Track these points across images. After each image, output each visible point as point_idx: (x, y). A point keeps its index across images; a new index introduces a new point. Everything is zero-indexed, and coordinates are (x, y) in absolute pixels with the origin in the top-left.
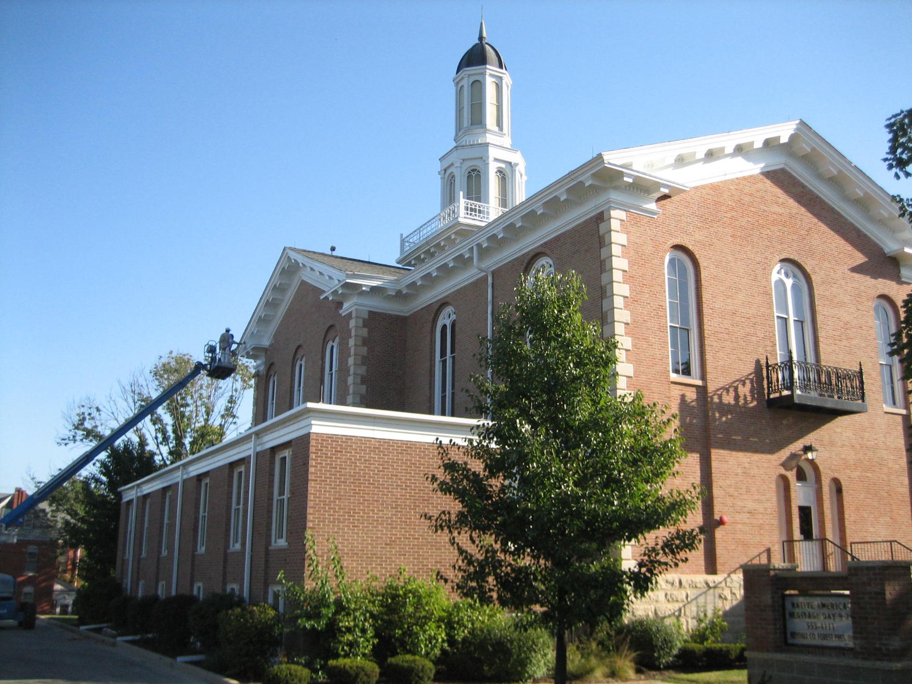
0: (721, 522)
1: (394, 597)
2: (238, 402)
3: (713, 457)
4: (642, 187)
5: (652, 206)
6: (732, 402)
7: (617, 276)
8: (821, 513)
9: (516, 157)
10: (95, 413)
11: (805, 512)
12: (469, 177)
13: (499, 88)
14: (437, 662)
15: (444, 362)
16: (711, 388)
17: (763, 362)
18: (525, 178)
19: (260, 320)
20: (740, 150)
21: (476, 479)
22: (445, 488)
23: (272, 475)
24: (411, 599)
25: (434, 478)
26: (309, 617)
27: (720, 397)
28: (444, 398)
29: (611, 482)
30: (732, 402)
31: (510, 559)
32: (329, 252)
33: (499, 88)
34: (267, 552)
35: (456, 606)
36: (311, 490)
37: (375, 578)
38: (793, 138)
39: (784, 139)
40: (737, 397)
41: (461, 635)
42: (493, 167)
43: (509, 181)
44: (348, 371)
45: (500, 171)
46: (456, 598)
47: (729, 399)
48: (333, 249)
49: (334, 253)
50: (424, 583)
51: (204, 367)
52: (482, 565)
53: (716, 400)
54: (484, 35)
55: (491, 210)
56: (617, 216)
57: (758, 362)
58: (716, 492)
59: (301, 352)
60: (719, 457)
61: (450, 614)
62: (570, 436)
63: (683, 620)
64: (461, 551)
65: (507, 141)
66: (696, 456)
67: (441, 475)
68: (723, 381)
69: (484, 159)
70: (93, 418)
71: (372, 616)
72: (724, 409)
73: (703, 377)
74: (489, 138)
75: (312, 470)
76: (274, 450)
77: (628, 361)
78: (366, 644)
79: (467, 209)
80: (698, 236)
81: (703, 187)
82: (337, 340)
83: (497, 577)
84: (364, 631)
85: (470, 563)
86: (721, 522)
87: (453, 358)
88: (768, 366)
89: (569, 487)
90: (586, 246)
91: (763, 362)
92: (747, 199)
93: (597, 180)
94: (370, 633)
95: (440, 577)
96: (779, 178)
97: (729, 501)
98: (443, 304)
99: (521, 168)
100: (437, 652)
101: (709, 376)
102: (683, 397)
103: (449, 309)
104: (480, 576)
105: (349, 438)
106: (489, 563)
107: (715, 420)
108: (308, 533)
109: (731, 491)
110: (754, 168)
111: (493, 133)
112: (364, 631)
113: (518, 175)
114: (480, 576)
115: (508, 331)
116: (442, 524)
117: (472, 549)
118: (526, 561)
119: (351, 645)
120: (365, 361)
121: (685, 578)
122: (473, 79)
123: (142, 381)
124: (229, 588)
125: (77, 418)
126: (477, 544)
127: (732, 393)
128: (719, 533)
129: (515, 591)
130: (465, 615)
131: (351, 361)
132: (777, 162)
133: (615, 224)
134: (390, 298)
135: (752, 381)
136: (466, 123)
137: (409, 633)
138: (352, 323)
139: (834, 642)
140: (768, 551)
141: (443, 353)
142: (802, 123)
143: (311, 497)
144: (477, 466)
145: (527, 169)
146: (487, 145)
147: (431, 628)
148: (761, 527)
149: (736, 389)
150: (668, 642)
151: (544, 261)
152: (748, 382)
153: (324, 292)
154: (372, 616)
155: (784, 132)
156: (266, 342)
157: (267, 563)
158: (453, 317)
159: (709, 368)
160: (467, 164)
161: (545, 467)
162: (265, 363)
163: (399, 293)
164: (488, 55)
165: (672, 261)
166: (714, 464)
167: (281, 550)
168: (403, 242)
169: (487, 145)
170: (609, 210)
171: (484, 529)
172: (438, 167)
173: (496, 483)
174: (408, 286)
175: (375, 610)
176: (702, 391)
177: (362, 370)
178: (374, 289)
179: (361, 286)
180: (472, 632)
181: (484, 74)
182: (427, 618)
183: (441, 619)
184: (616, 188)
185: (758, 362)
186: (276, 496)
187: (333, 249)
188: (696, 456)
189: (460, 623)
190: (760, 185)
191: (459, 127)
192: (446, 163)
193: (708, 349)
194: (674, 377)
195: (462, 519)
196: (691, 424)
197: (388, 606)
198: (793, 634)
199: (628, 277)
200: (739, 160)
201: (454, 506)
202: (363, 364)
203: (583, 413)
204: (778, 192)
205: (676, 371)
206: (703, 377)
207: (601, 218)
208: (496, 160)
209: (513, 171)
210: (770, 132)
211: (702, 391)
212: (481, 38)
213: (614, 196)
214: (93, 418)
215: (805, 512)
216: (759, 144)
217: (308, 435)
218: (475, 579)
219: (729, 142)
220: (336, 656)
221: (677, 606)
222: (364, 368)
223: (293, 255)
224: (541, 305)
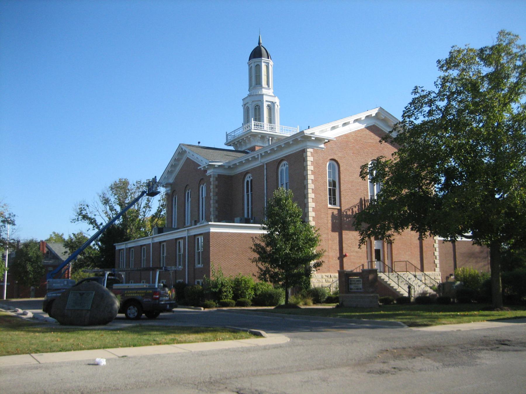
0: (346, 256)
1: (238, 282)
2: (151, 201)
3: (343, 233)
4: (319, 140)
5: (322, 146)
6: (351, 214)
7: (309, 172)
8: (384, 251)
9: (276, 100)
10: (86, 208)
11: (378, 252)
12: (255, 109)
13: (268, 67)
14: (252, 301)
15: (248, 195)
16: (343, 209)
17: (363, 199)
18: (279, 107)
19: (169, 171)
20: (356, 121)
21: (263, 248)
22: (254, 251)
23: (195, 244)
24: (243, 282)
25: (251, 248)
26: (214, 288)
27: (346, 212)
28: (248, 209)
29: (300, 249)
30: (351, 214)
31: (273, 270)
32: (197, 144)
33: (268, 67)
34: (194, 269)
35: (257, 284)
36: (211, 250)
37: (231, 276)
38: (376, 114)
39: (374, 115)
40: (353, 212)
41: (259, 293)
42: (265, 104)
43: (272, 111)
44: (211, 198)
45: (268, 106)
46: (258, 281)
47: (349, 213)
48: (199, 143)
49: (200, 145)
50: (247, 277)
51: (146, 192)
52: (265, 271)
53: (345, 213)
54: (261, 42)
55: (265, 125)
56: (310, 151)
57: (361, 199)
58: (344, 245)
59: (188, 187)
60: (345, 233)
61: (255, 287)
62: (287, 237)
63: (331, 288)
64: (259, 268)
65: (271, 92)
66: (337, 233)
67: (253, 247)
68: (348, 207)
69: (262, 101)
70: (85, 210)
71: (232, 287)
72: (347, 216)
73: (340, 206)
74: (264, 91)
75: (211, 243)
76: (195, 236)
77: (313, 202)
78: (231, 296)
79: (255, 125)
80: (340, 155)
81: (342, 136)
82: (205, 184)
83: (269, 275)
84: (230, 292)
85: (262, 271)
86: (346, 256)
87: (252, 194)
88: (364, 200)
89: (287, 251)
90: (298, 160)
91: (363, 199)
92: (359, 138)
93: (302, 138)
94: (232, 292)
95: (253, 275)
96: (372, 129)
97: (349, 248)
98: (247, 173)
99: (278, 103)
100: (251, 298)
101: (342, 205)
102: (333, 213)
103: (249, 175)
104: (264, 274)
105: (222, 233)
106: (267, 271)
107: (344, 220)
108: (211, 263)
109: (350, 245)
110: (362, 126)
111: (265, 88)
112: (230, 292)
113: (276, 106)
114: (264, 274)
115: (270, 207)
116: (254, 261)
117: (262, 267)
118: (277, 270)
119: (226, 296)
120: (217, 194)
121: (332, 275)
122: (256, 64)
123: (106, 192)
124: (177, 281)
125: (79, 211)
126: (263, 266)
127: (351, 211)
128: (345, 259)
129: (274, 278)
130: (260, 287)
131: (212, 194)
132: (371, 123)
133: (309, 154)
134: (225, 169)
135: (358, 206)
136: (254, 83)
137: (243, 292)
138: (212, 179)
139: (359, 290)
140: (363, 265)
141: (248, 192)
142: (381, 108)
143: (211, 252)
144: (263, 244)
145: (280, 103)
146: (263, 95)
147: (249, 291)
148: (360, 257)
149: (352, 209)
150: (323, 295)
151: (285, 162)
152: (357, 206)
153: (200, 166)
154: (232, 287)
155: (373, 112)
156: (171, 181)
157: (195, 273)
158: (251, 178)
159: (342, 203)
160: (254, 104)
161: (281, 246)
162: (171, 189)
163: (229, 167)
164: (263, 52)
165: (330, 164)
166: (344, 236)
167: (200, 268)
168: (227, 135)
169: (263, 95)
170: (307, 148)
171: (266, 262)
172: (242, 103)
173: (268, 249)
174: (233, 165)
175: (233, 285)
176: (340, 210)
177: (216, 198)
178: (219, 166)
179: (215, 165)
180: (262, 292)
181: (261, 62)
182: (248, 288)
183: (252, 288)
184: (309, 141)
185: (361, 199)
186: (196, 251)
187: (199, 143)
188: (337, 233)
189: (258, 289)
190: (364, 133)
191: (250, 85)
192: (246, 102)
193: (342, 195)
194: (329, 206)
195: (260, 259)
196: (335, 222)
197: (236, 284)
198: (351, 289)
199: (313, 173)
200: (357, 124)
201: (257, 256)
202: (216, 195)
203: (291, 231)
204: (372, 134)
205: (330, 203)
206: (340, 206)
207: (304, 151)
208: (267, 101)
209: (274, 106)
210: (368, 113)
211: (340, 210)
212: (259, 43)
213: (309, 144)
214: (85, 210)
215: (378, 252)
216: (363, 118)
217: (209, 232)
218: (263, 275)
219: (351, 119)
220: (222, 299)
221: (329, 284)
222: (217, 197)
223: (184, 148)
224: (280, 200)
